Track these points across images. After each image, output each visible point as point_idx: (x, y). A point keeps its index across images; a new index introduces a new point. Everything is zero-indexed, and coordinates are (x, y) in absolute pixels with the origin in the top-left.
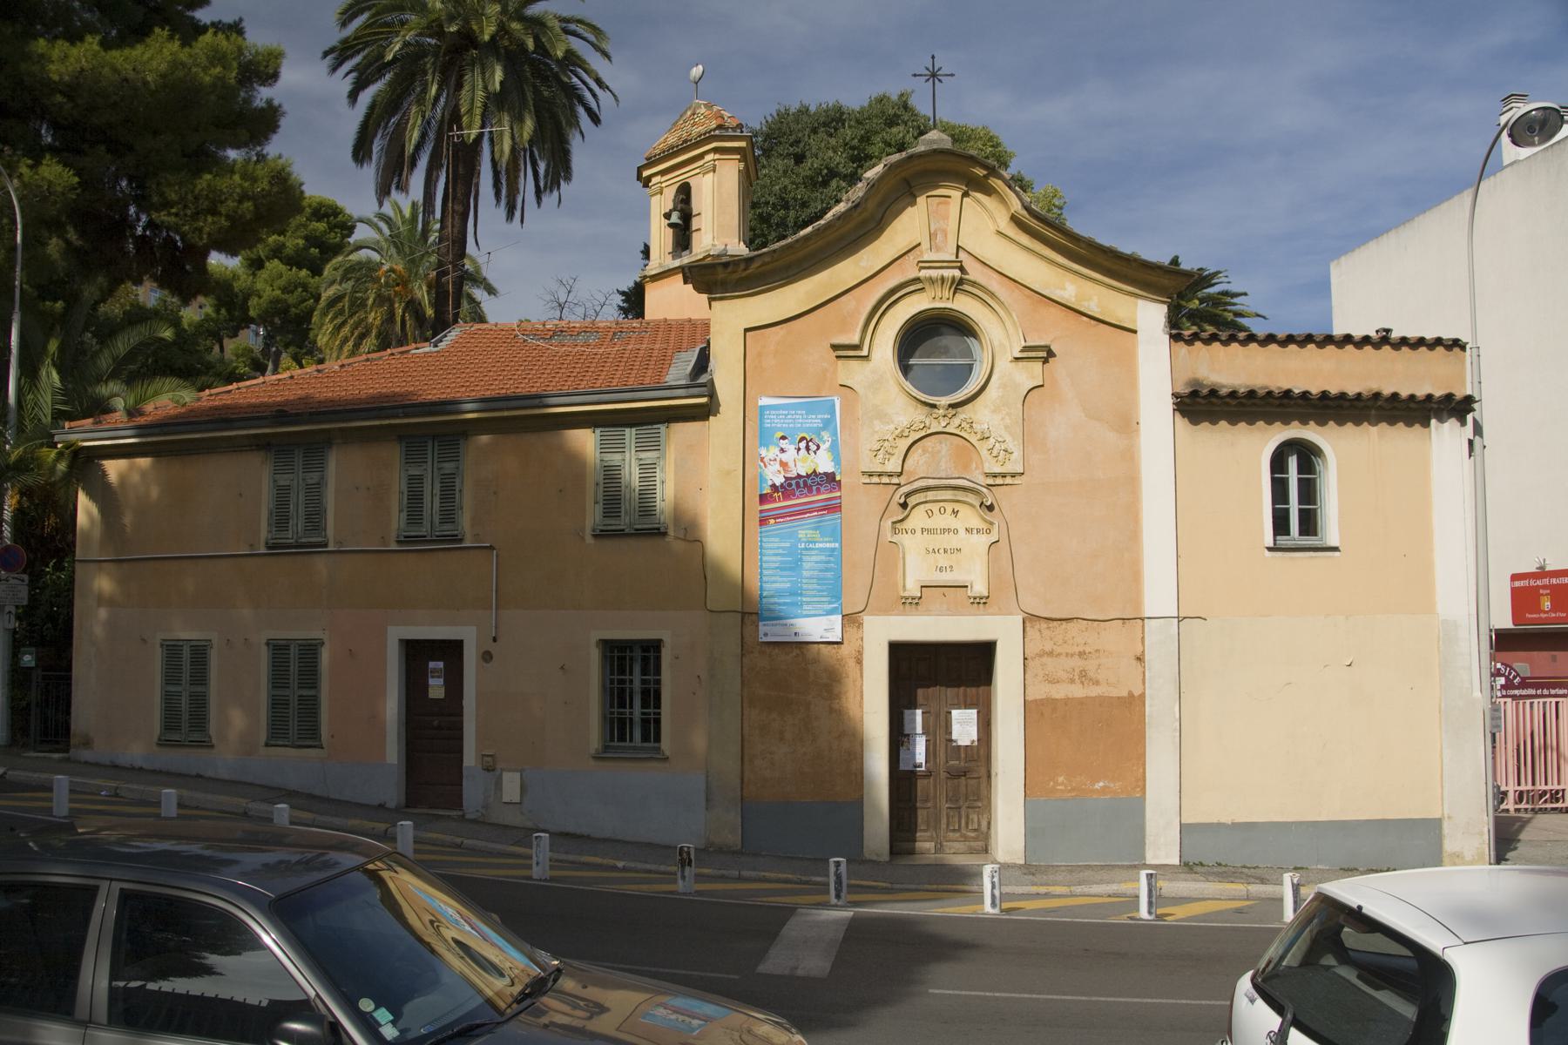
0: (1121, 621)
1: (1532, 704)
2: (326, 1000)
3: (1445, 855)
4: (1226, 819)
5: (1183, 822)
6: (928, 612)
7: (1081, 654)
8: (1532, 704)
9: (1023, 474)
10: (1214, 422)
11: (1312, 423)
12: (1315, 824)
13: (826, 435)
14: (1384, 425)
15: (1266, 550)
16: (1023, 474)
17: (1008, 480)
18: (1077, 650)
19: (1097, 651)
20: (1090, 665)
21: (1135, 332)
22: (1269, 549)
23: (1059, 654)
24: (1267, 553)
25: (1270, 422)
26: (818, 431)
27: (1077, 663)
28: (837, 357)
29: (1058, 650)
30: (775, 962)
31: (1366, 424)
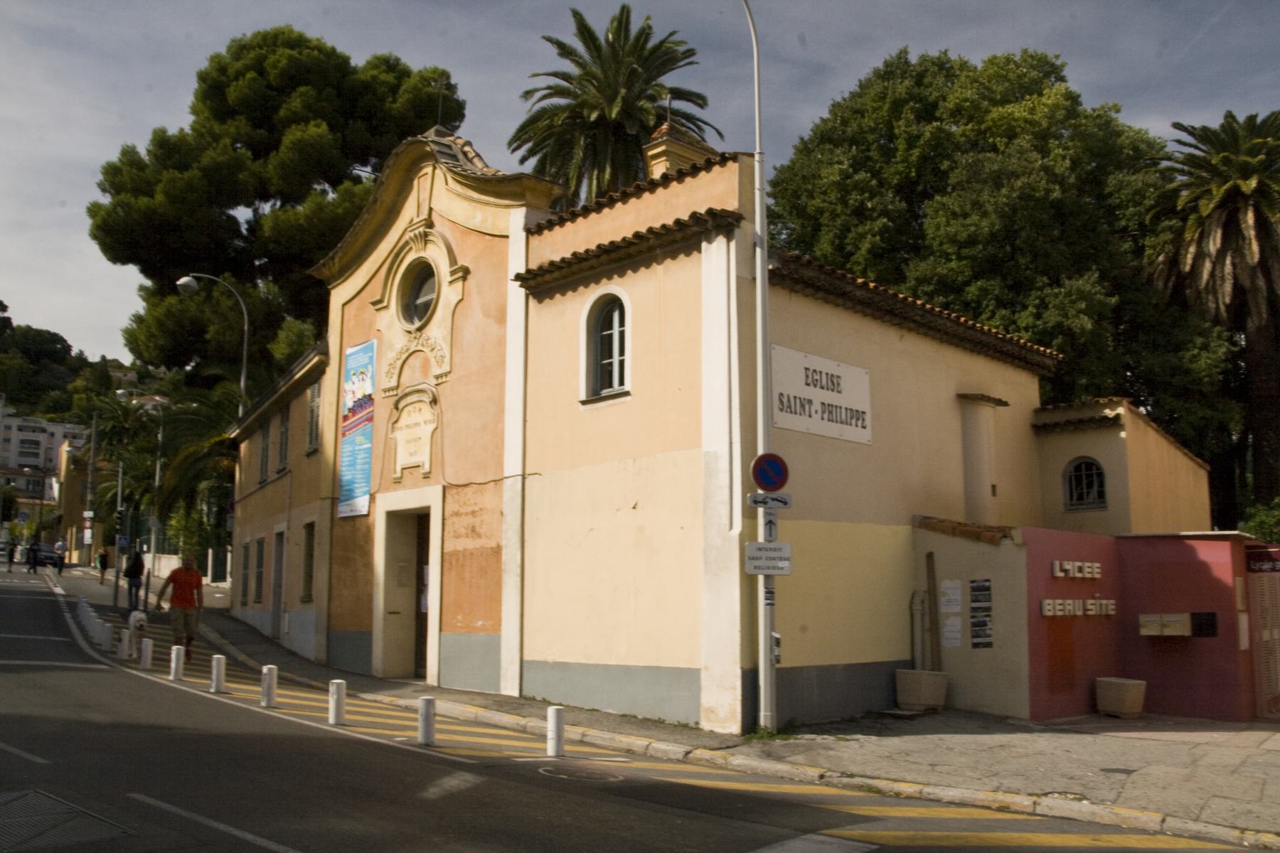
0: (493, 483)
1: (349, 712)
2: (273, 555)
3: (702, 708)
4: (550, 659)
5: (526, 658)
6: (404, 487)
7: (473, 513)
8: (349, 712)
9: (450, 372)
10: (552, 297)
11: (616, 277)
12: (606, 667)
13: (370, 367)
14: (668, 262)
15: (580, 404)
16: (450, 372)
17: (444, 379)
18: (470, 509)
19: (481, 509)
20: (476, 521)
21: (507, 237)
22: (584, 403)
23: (461, 514)
24: (582, 407)
25: (586, 286)
26: (366, 366)
27: (469, 520)
28: (377, 310)
29: (462, 510)
30: (1252, 562)
31: (654, 264)
